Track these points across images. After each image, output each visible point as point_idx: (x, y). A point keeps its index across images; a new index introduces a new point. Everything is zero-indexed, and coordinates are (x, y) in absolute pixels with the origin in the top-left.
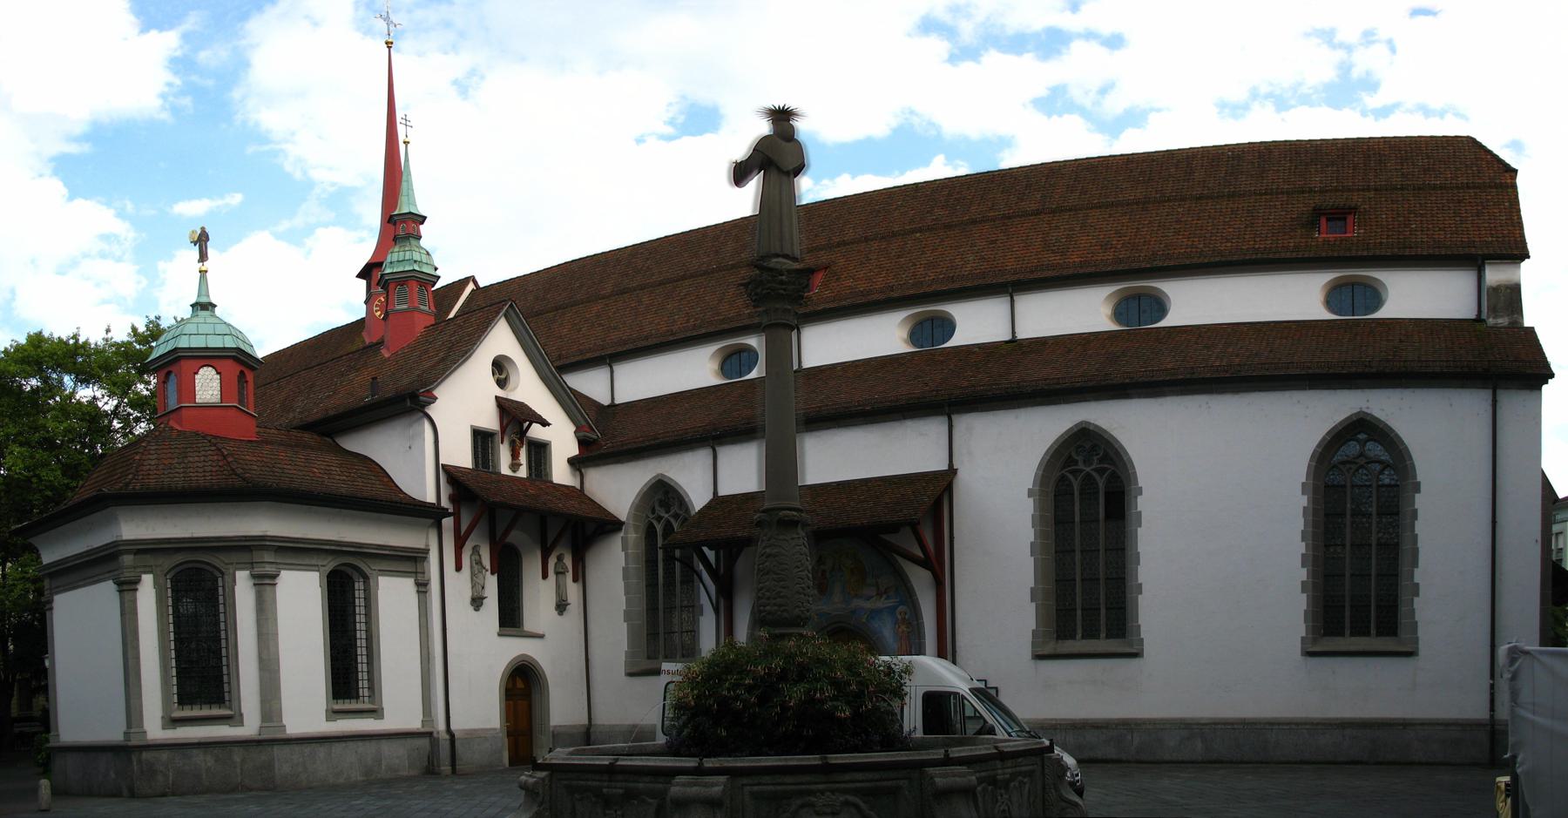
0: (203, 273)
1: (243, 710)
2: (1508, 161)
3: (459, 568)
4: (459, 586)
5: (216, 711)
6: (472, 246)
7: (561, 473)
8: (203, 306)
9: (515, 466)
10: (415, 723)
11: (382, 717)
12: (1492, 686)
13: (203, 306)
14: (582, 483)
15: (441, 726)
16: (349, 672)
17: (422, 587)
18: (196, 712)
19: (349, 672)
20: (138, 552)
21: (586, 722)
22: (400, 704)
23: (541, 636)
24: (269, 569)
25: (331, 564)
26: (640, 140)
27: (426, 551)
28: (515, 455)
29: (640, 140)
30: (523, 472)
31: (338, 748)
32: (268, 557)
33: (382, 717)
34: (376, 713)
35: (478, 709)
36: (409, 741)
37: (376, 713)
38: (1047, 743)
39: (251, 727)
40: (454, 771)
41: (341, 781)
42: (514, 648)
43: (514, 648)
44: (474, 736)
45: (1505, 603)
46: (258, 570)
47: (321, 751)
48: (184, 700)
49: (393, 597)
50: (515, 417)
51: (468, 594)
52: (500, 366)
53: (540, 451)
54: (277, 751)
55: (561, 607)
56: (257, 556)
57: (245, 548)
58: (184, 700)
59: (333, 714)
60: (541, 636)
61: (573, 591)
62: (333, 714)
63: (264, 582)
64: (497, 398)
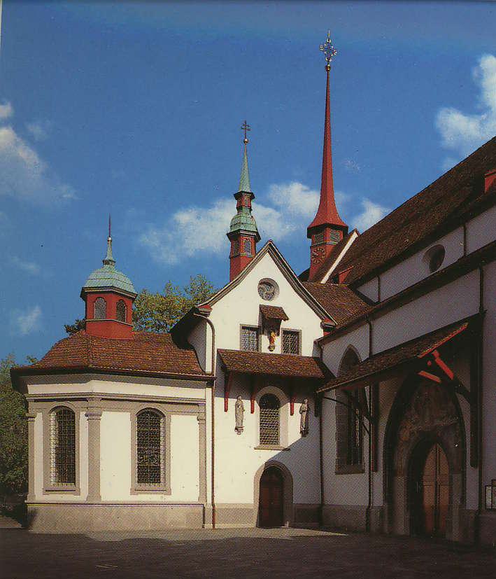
7: (307, 350)
10: (193, 496)
14: (321, 355)
15: (209, 501)
16: (150, 469)
17: (202, 421)
19: (150, 469)
20: (36, 401)
22: (182, 480)
28: (271, 340)
30: (278, 350)
31: (175, 508)
32: (94, 403)
34: (168, 491)
39: (82, 497)
40: (214, 526)
45: (325, 459)
49: (181, 433)
50: (271, 320)
52: (267, 286)
53: (293, 337)
56: (90, 403)
57: (82, 398)
61: (314, 421)
62: (135, 491)
63: (93, 417)
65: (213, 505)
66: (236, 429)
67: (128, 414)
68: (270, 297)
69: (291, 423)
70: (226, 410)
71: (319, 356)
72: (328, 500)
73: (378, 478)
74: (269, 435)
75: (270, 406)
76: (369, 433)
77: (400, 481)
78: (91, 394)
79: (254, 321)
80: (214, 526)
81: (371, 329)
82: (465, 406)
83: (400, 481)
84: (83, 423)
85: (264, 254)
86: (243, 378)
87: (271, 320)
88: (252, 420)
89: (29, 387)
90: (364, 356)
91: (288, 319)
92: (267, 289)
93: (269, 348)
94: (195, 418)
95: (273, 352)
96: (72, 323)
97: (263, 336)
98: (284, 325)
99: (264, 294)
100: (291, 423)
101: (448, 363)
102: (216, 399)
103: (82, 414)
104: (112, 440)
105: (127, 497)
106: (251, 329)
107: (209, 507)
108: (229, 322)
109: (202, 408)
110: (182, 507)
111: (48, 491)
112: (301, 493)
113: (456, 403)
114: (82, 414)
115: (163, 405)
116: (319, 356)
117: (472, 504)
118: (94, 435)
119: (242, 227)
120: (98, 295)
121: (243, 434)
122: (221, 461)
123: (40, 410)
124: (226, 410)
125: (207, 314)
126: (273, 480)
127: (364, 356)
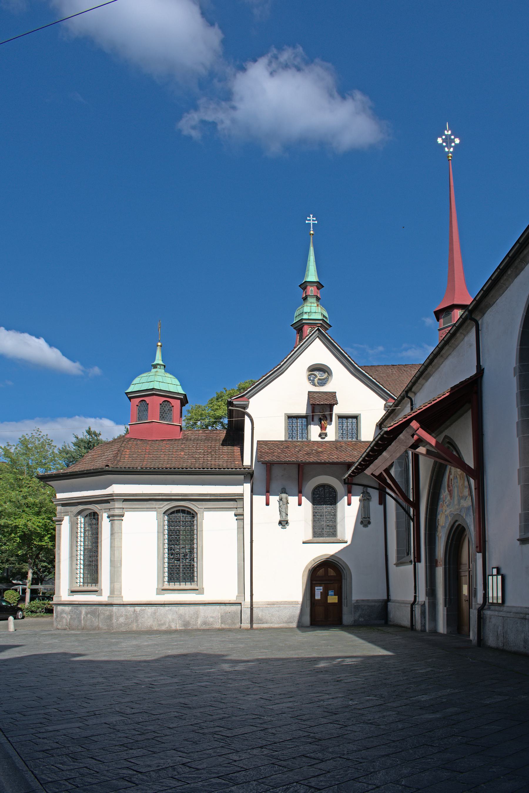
2: (454, 235)
5: (188, 586)
10: (232, 596)
11: (203, 593)
12: (415, 593)
17: (239, 516)
18: (177, 586)
20: (63, 505)
21: (386, 598)
24: (117, 512)
25: (167, 506)
27: (242, 495)
32: (117, 505)
33: (202, 593)
34: (198, 591)
36: (223, 607)
37: (198, 591)
38: (89, 616)
39: (104, 598)
40: (252, 626)
45: (332, 541)
46: (112, 513)
47: (150, 610)
48: (171, 579)
49: (215, 529)
50: (321, 408)
51: (278, 518)
52: (319, 371)
54: (115, 609)
58: (171, 579)
60: (303, 543)
66: (280, 523)
67: (155, 513)
68: (323, 383)
69: (348, 511)
72: (393, 597)
73: (422, 567)
74: (324, 529)
75: (324, 498)
77: (440, 571)
78: (111, 495)
79: (302, 409)
80: (252, 626)
83: (440, 571)
84: (105, 524)
86: (288, 471)
87: (321, 408)
89: (57, 495)
93: (320, 435)
94: (232, 513)
95: (327, 439)
96: (92, 430)
97: (312, 426)
98: (337, 410)
99: (316, 380)
100: (348, 511)
101: (164, 420)
103: (105, 515)
104: (137, 540)
105: (151, 595)
106: (297, 417)
108: (271, 412)
109: (239, 503)
110: (218, 607)
111: (73, 592)
112: (362, 589)
114: (105, 515)
119: (305, 317)
122: (263, 559)
123: (66, 513)
125: (245, 407)
126: (325, 575)
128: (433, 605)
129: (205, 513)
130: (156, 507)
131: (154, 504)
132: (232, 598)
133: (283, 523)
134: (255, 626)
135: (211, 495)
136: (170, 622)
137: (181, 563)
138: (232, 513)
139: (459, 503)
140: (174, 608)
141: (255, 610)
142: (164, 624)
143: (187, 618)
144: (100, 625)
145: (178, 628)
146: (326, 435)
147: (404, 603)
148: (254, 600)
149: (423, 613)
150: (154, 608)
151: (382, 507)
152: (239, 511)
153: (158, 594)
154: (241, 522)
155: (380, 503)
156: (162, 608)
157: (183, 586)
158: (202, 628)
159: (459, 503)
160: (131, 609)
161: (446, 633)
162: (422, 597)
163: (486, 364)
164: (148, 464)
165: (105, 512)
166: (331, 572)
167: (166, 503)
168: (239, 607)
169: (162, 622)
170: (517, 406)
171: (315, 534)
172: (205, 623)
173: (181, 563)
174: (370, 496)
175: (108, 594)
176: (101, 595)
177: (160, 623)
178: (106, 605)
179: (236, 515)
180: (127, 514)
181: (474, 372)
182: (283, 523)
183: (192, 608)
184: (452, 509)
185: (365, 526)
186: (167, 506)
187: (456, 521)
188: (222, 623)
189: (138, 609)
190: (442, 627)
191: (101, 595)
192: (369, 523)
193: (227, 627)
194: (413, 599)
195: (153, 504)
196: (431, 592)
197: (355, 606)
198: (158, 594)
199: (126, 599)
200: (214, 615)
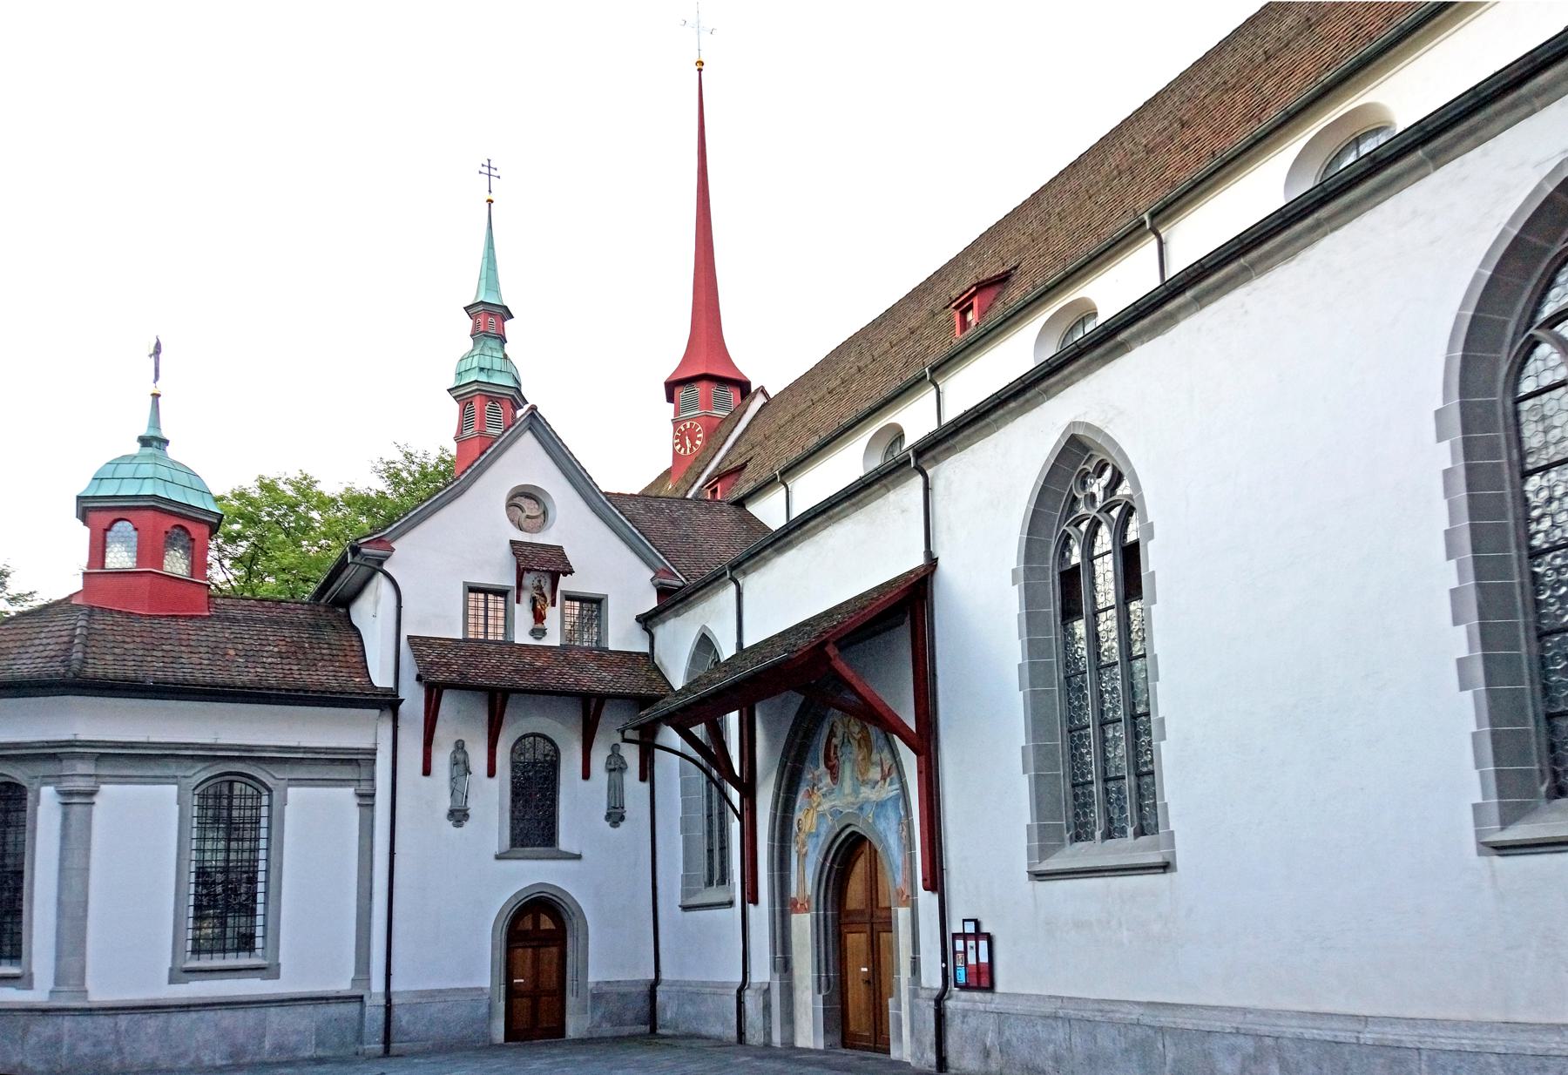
0: (156, 396)
1: (34, 969)
3: (491, 772)
4: (425, 797)
5: (244, 960)
6: (774, 350)
8: (153, 441)
9: (538, 632)
11: (277, 976)
13: (153, 441)
15: (378, 986)
17: (367, 799)
22: (311, 939)
23: (578, 857)
24: (81, 784)
25: (200, 773)
26: (489, 170)
27: (373, 752)
28: (539, 617)
29: (489, 170)
32: (82, 767)
33: (277, 976)
35: (452, 957)
37: (268, 971)
39: (39, 994)
41: (183, 1064)
42: (533, 873)
43: (533, 873)
44: (693, 993)
46: (68, 785)
47: (153, 1023)
49: (311, 830)
51: (446, 804)
52: (526, 501)
55: (616, 816)
56: (67, 767)
57: (52, 754)
59: (179, 974)
60: (578, 857)
62: (179, 974)
63: (77, 800)
64: (512, 542)
65: (388, 1008)
67: (173, 789)
70: (427, 771)
71: (647, 650)
73: (761, 914)
76: (740, 818)
77: (803, 925)
81: (927, 489)
82: (909, 760)
85: (523, 432)
87: (541, 568)
88: (492, 798)
90: (727, 650)
91: (571, 572)
92: (530, 507)
95: (545, 642)
102: (390, 684)
103: (48, 792)
107: (374, 1011)
113: (894, 753)
114: (48, 792)
115: (271, 769)
116: (647, 650)
117: (972, 960)
118: (75, 841)
120: (117, 515)
121: (467, 825)
124: (427, 771)
127: (727, 650)
128: (788, 991)
129: (290, 790)
130: (178, 774)
131: (173, 769)
132: (344, 986)
133: (458, 816)
134: (394, 1046)
135: (306, 750)
136: (198, 1048)
137: (226, 903)
138: (349, 792)
139: (856, 792)
140: (209, 1015)
141: (396, 1012)
142: (183, 1055)
143: (241, 1038)
144: (29, 1064)
145: (219, 1062)
146: (543, 632)
147: (725, 985)
148: (393, 988)
149: (767, 1007)
150: (162, 1017)
151: (647, 785)
152: (365, 788)
153: (171, 981)
154: (367, 811)
155: (643, 779)
156: (181, 1015)
157: (231, 961)
158: (273, 1059)
159: (856, 792)
160: (105, 1022)
161: (821, 1046)
162: (762, 972)
163: (940, 552)
164: (155, 670)
165: (47, 784)
166: (547, 923)
167: (200, 766)
168: (353, 1008)
169: (182, 1048)
170: (1020, 637)
171: (515, 842)
172: (280, 1047)
173: (226, 903)
174: (624, 763)
175: (50, 985)
176: (30, 986)
177: (175, 1051)
178: (45, 1011)
179: (360, 796)
180: (103, 787)
181: (918, 560)
182: (458, 816)
183: (251, 1015)
184: (836, 802)
185: (615, 824)
186: (200, 773)
187: (848, 826)
188: (317, 1046)
189: (123, 1021)
190: (809, 1033)
191: (30, 986)
192: (622, 818)
193: (329, 1053)
194: (740, 979)
195: (167, 766)
196: (784, 964)
197: (594, 996)
198: (171, 981)
199: (99, 993)
200: (301, 1028)
